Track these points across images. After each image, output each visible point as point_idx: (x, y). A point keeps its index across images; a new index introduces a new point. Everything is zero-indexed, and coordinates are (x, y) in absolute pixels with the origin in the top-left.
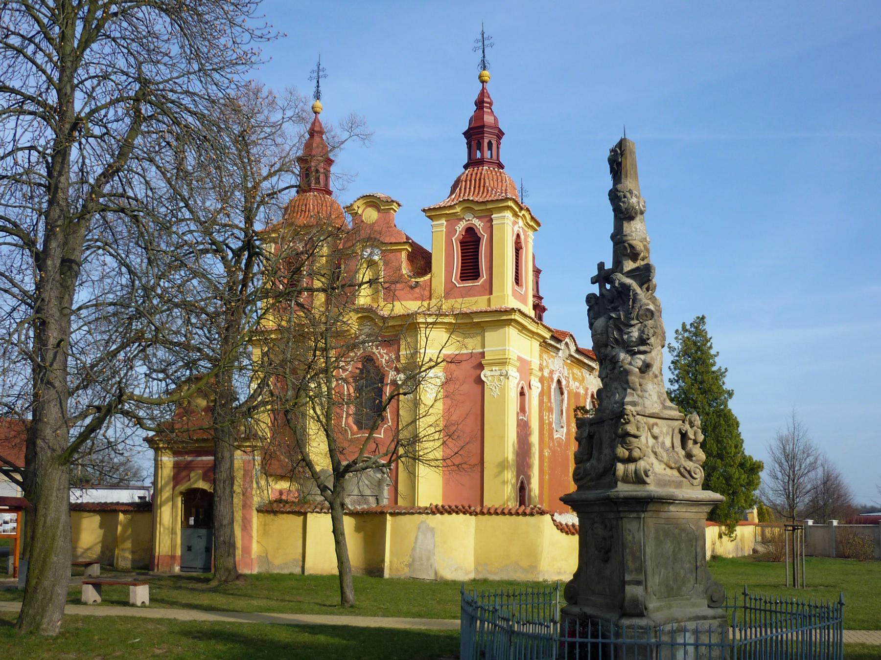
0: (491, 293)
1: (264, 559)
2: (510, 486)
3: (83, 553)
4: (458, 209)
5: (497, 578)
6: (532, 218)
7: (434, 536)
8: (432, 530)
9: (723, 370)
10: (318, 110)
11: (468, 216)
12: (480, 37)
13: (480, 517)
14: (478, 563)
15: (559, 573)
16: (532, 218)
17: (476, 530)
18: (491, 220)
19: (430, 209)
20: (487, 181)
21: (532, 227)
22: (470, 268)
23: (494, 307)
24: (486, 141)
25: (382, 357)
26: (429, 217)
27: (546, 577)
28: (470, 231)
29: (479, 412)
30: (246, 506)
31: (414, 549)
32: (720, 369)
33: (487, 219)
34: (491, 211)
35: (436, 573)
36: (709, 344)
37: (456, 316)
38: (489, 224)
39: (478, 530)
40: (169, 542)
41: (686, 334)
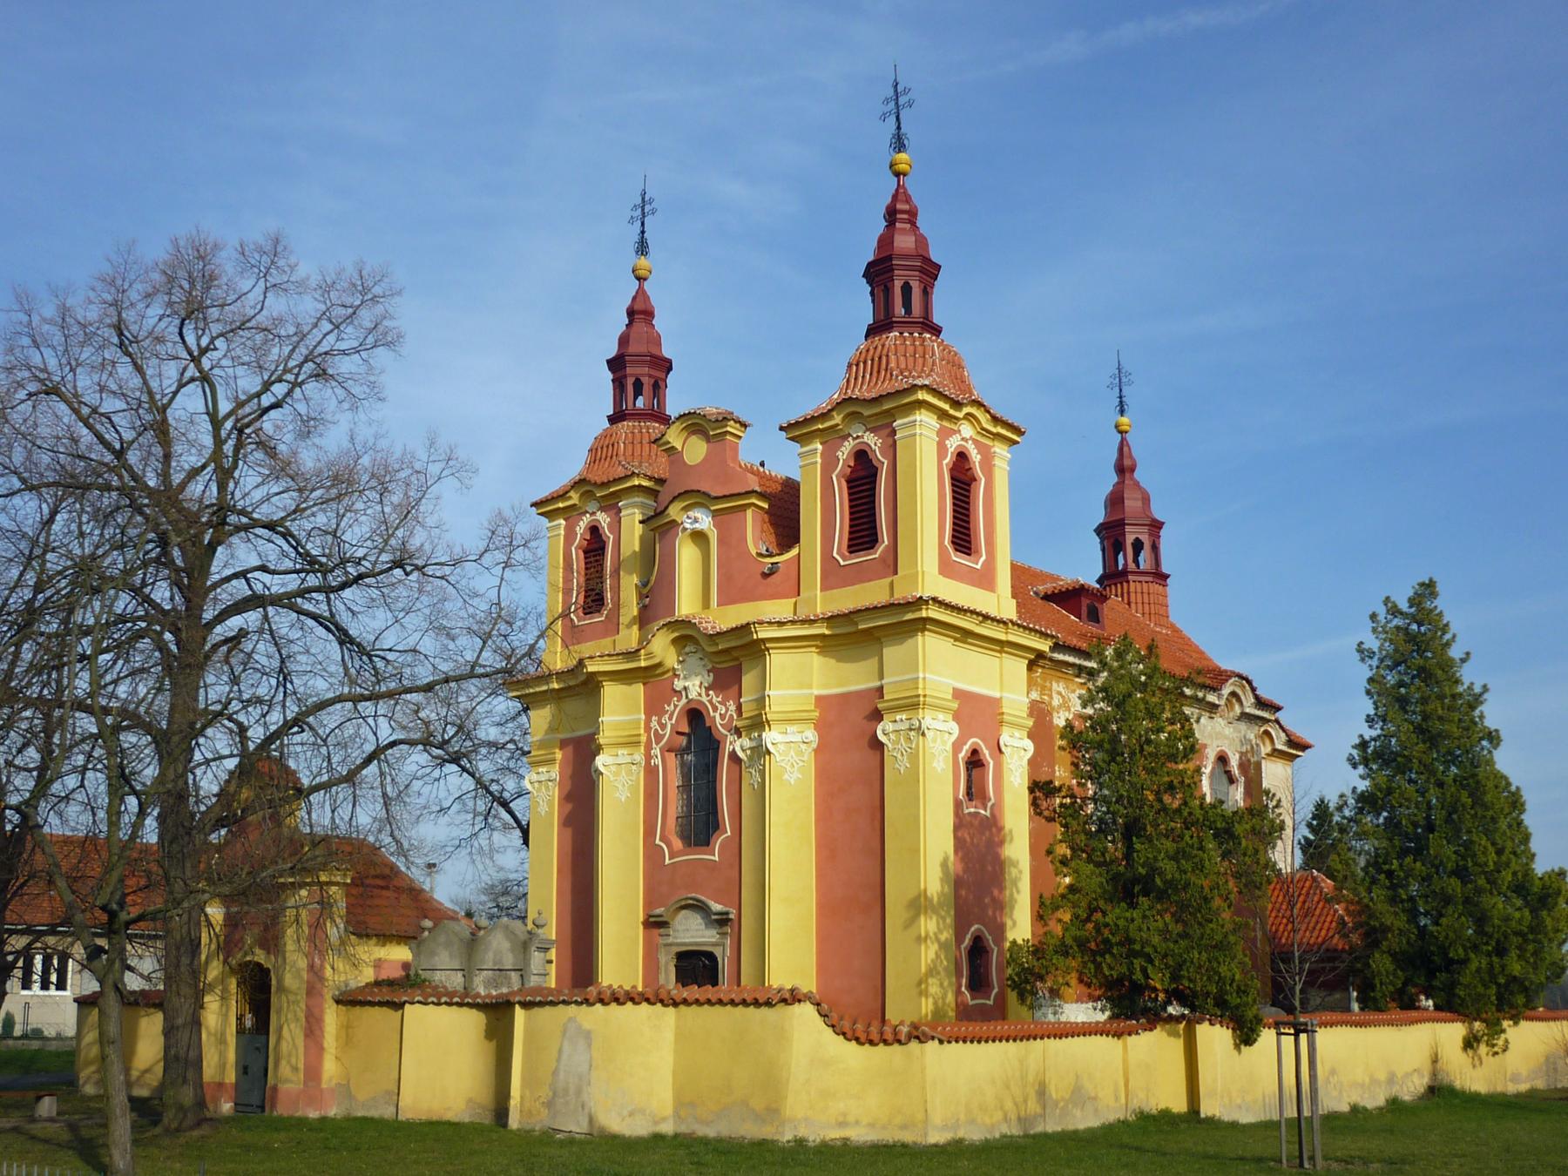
0: (896, 573)
1: (345, 1090)
2: (934, 948)
3: (139, 1078)
4: (837, 419)
5: (711, 1132)
6: (995, 420)
7: (590, 1045)
8: (588, 1036)
9: (1477, 689)
10: (642, 273)
11: (857, 430)
12: (891, 92)
13: (683, 1008)
14: (680, 1104)
15: (842, 1124)
16: (995, 420)
17: (677, 1035)
18: (894, 432)
19: (797, 424)
20: (893, 357)
21: (998, 436)
22: (863, 533)
23: (900, 595)
24: (898, 284)
25: (715, 709)
26: (791, 439)
27: (802, 1132)
28: (862, 456)
29: (878, 803)
30: (313, 990)
31: (555, 1073)
32: (1470, 688)
33: (888, 431)
34: (891, 414)
35: (591, 1120)
36: (1448, 636)
37: (831, 620)
38: (890, 441)
39: (680, 1036)
40: (216, 1058)
41: (1397, 622)
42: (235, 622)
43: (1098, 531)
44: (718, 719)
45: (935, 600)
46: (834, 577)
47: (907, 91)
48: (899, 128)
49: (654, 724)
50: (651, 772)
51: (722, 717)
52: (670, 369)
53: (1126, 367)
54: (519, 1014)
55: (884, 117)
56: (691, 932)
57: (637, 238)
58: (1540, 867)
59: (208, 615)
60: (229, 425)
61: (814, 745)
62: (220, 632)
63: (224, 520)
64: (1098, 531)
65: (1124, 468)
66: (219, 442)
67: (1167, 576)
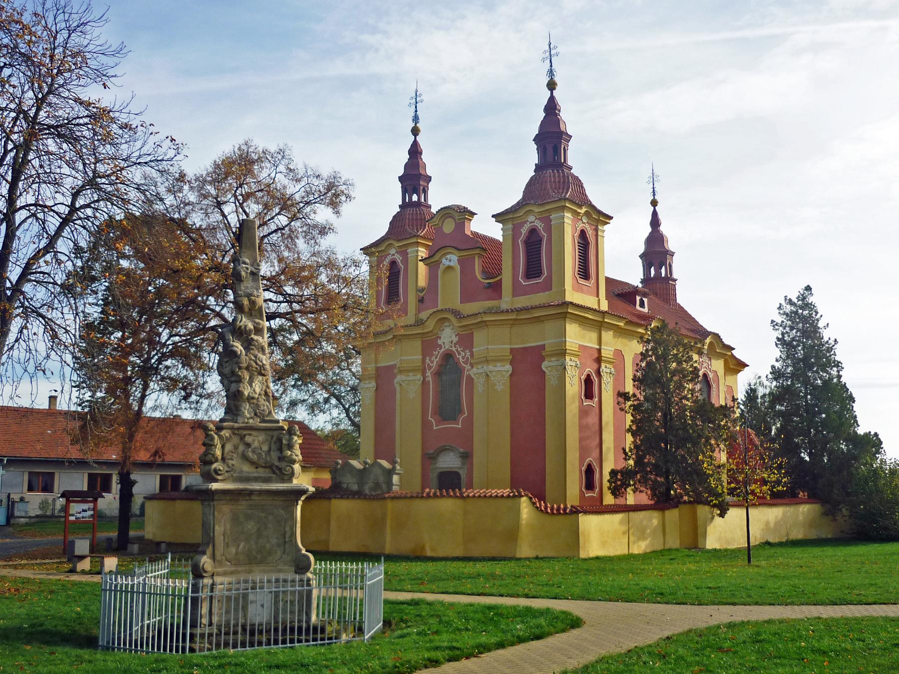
22: (533, 269)
25: (459, 354)
29: (597, 428)
36: (818, 316)
43: (641, 257)
45: (571, 303)
46: (517, 291)
49: (427, 361)
50: (424, 383)
51: (463, 358)
54: (85, 489)
55: (543, 60)
56: (449, 462)
57: (413, 114)
58: (861, 431)
65: (655, 222)
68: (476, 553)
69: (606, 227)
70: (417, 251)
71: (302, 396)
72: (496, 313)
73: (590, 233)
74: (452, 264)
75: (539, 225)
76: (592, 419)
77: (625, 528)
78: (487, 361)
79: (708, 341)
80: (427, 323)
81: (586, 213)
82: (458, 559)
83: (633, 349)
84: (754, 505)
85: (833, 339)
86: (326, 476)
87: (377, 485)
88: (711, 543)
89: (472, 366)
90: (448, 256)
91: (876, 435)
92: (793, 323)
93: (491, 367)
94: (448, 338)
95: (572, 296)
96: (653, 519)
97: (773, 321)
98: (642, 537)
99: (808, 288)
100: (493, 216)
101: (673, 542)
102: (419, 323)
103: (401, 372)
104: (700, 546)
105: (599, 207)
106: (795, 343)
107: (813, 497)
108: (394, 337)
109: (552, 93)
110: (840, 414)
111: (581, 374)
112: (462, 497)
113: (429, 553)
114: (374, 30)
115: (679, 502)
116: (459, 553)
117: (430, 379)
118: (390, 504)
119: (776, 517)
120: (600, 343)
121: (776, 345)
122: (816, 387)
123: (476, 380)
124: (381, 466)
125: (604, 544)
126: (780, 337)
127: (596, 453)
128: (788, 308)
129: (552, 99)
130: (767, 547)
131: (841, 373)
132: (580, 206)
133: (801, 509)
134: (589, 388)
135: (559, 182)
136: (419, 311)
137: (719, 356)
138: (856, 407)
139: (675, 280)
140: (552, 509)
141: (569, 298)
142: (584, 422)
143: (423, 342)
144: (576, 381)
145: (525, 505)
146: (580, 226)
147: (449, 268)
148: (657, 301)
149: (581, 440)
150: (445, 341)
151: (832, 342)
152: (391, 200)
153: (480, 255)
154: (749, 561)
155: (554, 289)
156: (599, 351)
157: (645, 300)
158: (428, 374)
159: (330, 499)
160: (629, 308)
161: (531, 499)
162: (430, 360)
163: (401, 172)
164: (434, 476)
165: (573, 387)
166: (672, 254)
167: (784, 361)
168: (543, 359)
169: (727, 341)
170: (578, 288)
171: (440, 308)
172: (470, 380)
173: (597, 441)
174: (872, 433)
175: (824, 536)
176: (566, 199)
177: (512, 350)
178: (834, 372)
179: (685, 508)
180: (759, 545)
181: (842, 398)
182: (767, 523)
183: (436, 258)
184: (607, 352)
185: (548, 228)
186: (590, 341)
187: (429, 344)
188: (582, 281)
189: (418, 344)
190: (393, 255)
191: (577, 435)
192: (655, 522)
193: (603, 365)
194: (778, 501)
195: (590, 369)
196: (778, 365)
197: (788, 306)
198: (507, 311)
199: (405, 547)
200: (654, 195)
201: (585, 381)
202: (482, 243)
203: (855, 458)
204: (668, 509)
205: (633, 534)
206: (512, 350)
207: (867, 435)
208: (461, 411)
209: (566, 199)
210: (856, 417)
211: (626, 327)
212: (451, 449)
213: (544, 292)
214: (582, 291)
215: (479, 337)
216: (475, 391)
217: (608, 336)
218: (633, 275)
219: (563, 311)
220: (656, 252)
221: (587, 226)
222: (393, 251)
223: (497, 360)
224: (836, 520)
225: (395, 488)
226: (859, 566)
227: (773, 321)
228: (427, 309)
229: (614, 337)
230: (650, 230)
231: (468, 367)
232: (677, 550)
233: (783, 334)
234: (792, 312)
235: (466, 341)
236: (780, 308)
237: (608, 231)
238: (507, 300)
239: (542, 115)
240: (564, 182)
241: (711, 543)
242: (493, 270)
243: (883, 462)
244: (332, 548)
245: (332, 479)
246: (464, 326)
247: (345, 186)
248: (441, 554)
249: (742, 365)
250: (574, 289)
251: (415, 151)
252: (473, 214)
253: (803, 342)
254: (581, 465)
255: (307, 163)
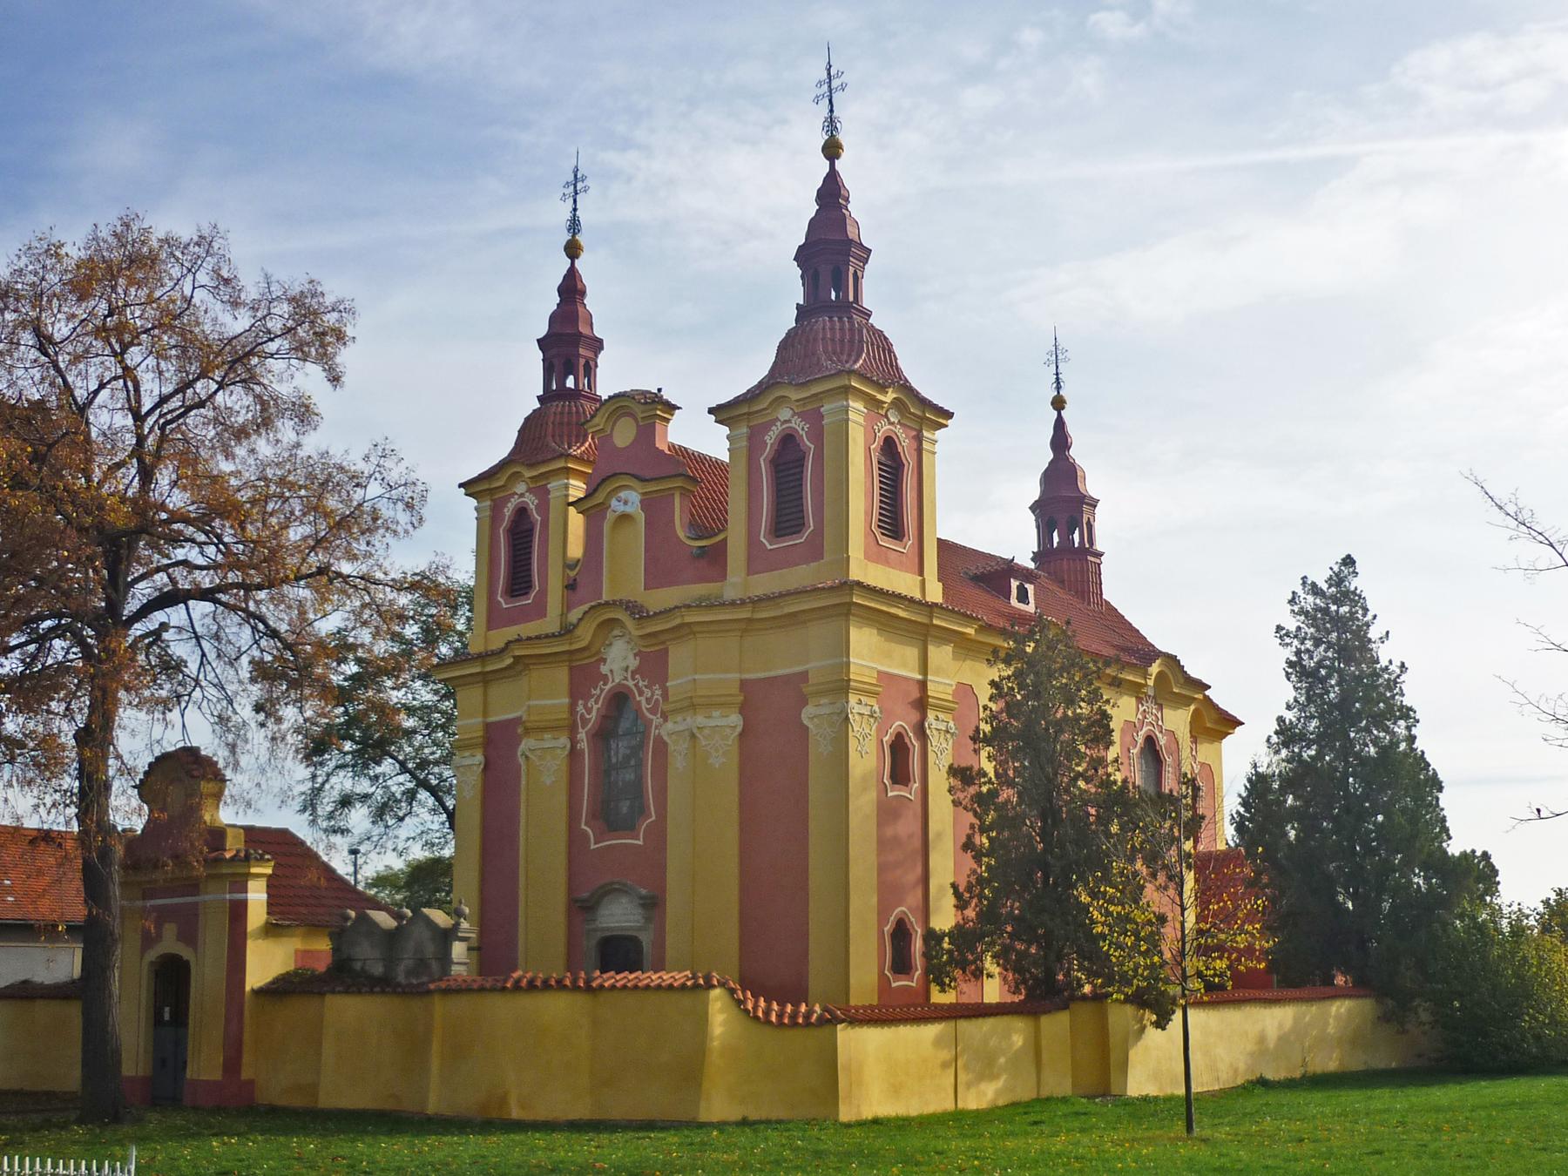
22: (787, 518)
29: (917, 843)
36: (1369, 617)
42: (159, 617)
43: (1033, 508)
44: (644, 705)
45: (859, 584)
46: (757, 561)
47: (840, 74)
48: (831, 111)
49: (580, 708)
50: (574, 754)
52: (601, 348)
53: (1062, 344)
56: (619, 915)
57: (569, 215)
58: (1454, 848)
59: (132, 606)
60: (151, 420)
61: (739, 729)
62: (138, 629)
63: (148, 525)
64: (1033, 508)
65: (1060, 440)
66: (141, 440)
67: (1101, 554)
68: (616, 1113)
69: (939, 434)
70: (567, 487)
71: (364, 786)
72: (712, 606)
73: (905, 443)
74: (629, 509)
75: (800, 427)
76: (907, 826)
77: (946, 1055)
78: (692, 706)
79: (1155, 669)
80: (578, 632)
81: (896, 403)
82: (576, 1126)
83: (982, 677)
84: (1199, 1004)
85: (1397, 663)
86: (323, 945)
87: (421, 964)
88: (1138, 1084)
89: (665, 717)
90: (623, 494)
91: (1486, 856)
92: (1318, 630)
93: (700, 720)
94: (619, 660)
95: (862, 569)
96: (1017, 1033)
97: (1279, 628)
98: (986, 1070)
99: (1349, 561)
100: (711, 411)
101: (1059, 1083)
102: (567, 630)
103: (528, 731)
104: (1115, 1090)
105: (926, 392)
106: (1323, 672)
107: (1361, 986)
108: (517, 659)
109: (832, 166)
110: (1414, 818)
111: (881, 732)
112: (589, 988)
113: (516, 1113)
114: (626, 144)
115: (1073, 998)
116: (581, 1112)
117: (584, 745)
118: (439, 1006)
119: (1280, 1025)
120: (924, 668)
121: (1288, 676)
122: (1364, 761)
123: (671, 748)
124: (429, 922)
125: (896, 1090)
126: (1294, 659)
127: (914, 898)
128: (1309, 601)
129: (832, 179)
130: (1259, 1090)
131: (1414, 731)
132: (883, 388)
133: (1334, 1009)
134: (900, 760)
135: (842, 341)
136: (568, 606)
137: (1184, 701)
138: (1445, 799)
139: (1099, 555)
140: (780, 1016)
141: (855, 574)
142: (889, 832)
143: (571, 669)
144: (871, 746)
145: (718, 1005)
146: (883, 429)
147: (625, 518)
148: (1061, 594)
149: (882, 869)
150: (615, 667)
151: (1395, 668)
152: (523, 385)
153: (685, 492)
154: (1189, 1128)
155: (828, 557)
156: (923, 685)
157: (1030, 588)
158: (582, 734)
159: (322, 994)
160: (998, 603)
161: (732, 991)
162: (585, 706)
163: (542, 330)
164: (590, 945)
165: (865, 757)
166: (1093, 503)
167: (1303, 708)
168: (804, 702)
169: (1193, 671)
170: (876, 555)
171: (605, 597)
172: (661, 747)
173: (919, 870)
174: (1478, 854)
175: (1382, 1066)
176: (851, 372)
177: (744, 685)
178: (1400, 728)
179: (1085, 1011)
180: (1243, 1087)
181: (1421, 783)
182: (1262, 1039)
183: (599, 497)
184: (941, 687)
185: (817, 435)
186: (904, 665)
187: (583, 675)
188: (886, 542)
189: (562, 675)
190: (522, 495)
191: (872, 859)
192: (1018, 1040)
193: (931, 715)
194: (1247, 994)
195: (903, 722)
196: (1290, 716)
197: (1310, 598)
198: (733, 603)
199: (466, 1101)
200: (1058, 388)
201: (893, 746)
202: (689, 468)
203: (1445, 903)
204: (1047, 1012)
205: (966, 1067)
206: (744, 685)
207: (1464, 855)
208: (642, 811)
209: (851, 372)
210: (1444, 819)
211: (982, 638)
212: (623, 890)
213: (807, 562)
214: (887, 563)
215: (679, 656)
216: (671, 772)
217: (940, 655)
218: (1012, 536)
219: (845, 601)
220: (1063, 501)
221: (899, 430)
222: (521, 488)
223: (710, 704)
224: (1405, 1032)
225: (455, 969)
226: (1427, 1137)
227: (1279, 628)
228: (581, 603)
229: (956, 657)
230: (1049, 455)
231: (656, 720)
232: (1064, 1100)
233: (1298, 653)
234: (1317, 609)
235: (654, 665)
236: (1292, 601)
237: (944, 444)
238: (737, 582)
239: (812, 209)
240: (851, 341)
241: (1138, 1084)
242: (709, 523)
243: (1496, 913)
244: (326, 1101)
245: (336, 950)
246: (649, 635)
247: (335, 315)
248: (541, 1114)
249: (1231, 723)
250: (868, 556)
251: (571, 289)
252: (671, 408)
253: (1340, 671)
254: (882, 921)
255: (270, 271)
